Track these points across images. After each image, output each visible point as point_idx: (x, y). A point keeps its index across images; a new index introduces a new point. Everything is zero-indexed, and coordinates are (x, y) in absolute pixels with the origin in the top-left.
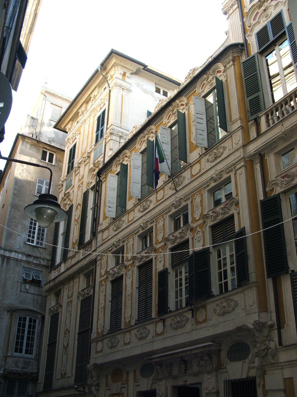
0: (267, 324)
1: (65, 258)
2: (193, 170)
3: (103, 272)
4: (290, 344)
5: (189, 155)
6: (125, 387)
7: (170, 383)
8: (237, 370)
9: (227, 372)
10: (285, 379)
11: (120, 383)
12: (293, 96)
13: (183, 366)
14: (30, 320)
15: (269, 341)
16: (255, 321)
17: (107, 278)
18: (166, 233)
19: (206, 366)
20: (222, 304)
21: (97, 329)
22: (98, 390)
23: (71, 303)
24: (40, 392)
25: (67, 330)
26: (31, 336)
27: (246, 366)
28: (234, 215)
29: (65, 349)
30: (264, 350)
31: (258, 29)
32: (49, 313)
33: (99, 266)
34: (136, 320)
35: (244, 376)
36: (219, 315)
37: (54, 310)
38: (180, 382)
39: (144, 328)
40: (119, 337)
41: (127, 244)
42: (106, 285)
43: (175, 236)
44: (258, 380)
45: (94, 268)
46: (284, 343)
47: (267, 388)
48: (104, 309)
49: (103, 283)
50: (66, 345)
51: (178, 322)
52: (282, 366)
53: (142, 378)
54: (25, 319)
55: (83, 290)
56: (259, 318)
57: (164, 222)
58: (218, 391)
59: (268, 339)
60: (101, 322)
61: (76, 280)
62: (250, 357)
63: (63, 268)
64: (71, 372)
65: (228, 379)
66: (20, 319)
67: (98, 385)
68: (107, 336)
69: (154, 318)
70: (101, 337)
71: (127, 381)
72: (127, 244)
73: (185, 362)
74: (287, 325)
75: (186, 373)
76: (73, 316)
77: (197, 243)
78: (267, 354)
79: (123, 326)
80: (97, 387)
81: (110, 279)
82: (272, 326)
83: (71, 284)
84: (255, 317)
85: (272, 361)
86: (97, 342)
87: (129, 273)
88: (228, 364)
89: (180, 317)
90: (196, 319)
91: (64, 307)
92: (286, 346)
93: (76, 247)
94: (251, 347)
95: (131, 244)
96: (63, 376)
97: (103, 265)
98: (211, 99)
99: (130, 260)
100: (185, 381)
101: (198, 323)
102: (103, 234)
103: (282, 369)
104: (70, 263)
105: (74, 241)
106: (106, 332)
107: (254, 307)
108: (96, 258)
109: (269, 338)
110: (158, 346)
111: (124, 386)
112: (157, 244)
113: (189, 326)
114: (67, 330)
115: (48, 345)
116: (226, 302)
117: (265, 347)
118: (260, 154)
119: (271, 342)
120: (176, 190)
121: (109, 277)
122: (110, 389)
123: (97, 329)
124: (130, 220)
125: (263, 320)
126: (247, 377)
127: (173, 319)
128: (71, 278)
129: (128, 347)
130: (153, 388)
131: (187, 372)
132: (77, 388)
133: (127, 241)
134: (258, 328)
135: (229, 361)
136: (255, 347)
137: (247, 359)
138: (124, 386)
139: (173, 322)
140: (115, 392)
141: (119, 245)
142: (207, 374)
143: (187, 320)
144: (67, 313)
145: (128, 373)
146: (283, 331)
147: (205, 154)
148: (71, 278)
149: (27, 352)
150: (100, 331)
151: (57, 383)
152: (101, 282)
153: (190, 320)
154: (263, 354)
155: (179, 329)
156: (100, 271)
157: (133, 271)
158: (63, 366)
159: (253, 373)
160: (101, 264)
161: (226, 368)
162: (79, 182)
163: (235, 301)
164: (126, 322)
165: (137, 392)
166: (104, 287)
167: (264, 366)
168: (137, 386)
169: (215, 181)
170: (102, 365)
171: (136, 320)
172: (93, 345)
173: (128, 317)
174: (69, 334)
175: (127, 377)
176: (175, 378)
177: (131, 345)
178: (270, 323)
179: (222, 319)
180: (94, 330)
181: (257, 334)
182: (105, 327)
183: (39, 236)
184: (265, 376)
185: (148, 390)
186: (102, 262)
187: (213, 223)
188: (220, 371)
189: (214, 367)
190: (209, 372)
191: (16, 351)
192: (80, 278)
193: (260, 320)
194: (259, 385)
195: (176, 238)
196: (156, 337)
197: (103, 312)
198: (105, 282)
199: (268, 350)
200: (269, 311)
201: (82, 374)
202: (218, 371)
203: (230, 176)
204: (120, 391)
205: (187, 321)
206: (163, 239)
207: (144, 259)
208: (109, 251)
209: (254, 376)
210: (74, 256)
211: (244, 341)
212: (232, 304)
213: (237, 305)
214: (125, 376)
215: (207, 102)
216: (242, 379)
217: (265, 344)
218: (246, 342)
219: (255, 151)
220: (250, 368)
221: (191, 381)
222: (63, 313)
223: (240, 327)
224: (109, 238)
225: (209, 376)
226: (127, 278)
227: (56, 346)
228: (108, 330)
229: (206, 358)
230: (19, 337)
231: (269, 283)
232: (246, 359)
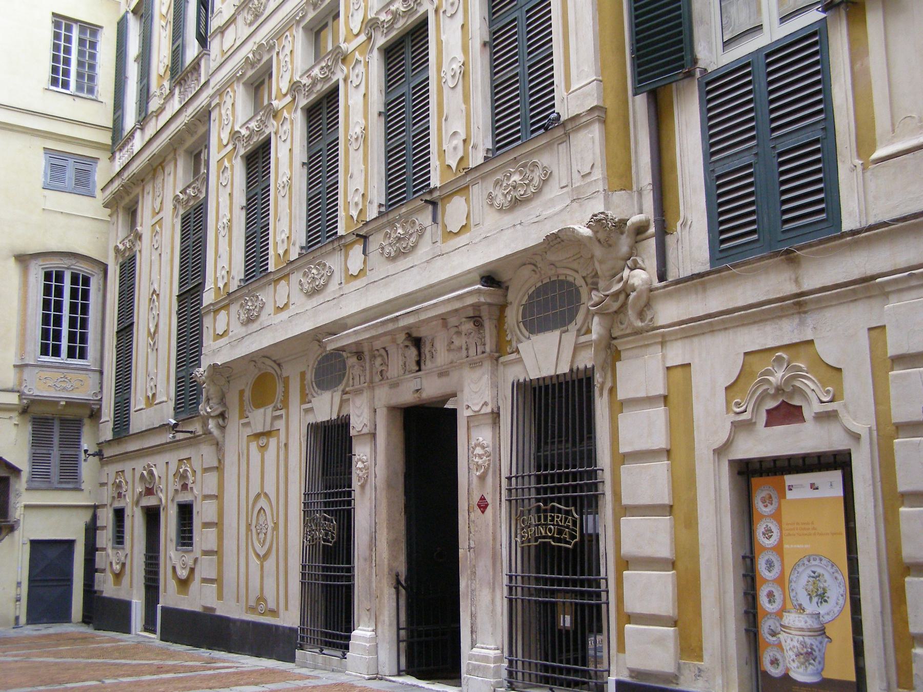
0: (629, 223)
1: (144, 118)
3: (225, 137)
4: (688, 273)
6: (281, 416)
7: (384, 396)
8: (545, 356)
9: (520, 360)
10: (668, 368)
11: (269, 409)
13: (413, 352)
14: (75, 279)
15: (632, 269)
16: (596, 215)
17: (235, 148)
18: (372, 8)
19: (467, 349)
20: (509, 178)
21: (216, 279)
22: (222, 428)
23: (161, 227)
24: (106, 442)
25: (154, 291)
26: (78, 330)
27: (570, 338)
29: (153, 339)
30: (616, 295)
32: (116, 257)
33: (217, 121)
34: (302, 248)
35: (564, 369)
36: (501, 210)
37: (125, 250)
38: (406, 396)
40: (262, 296)
41: (278, 54)
42: (232, 167)
43: (392, 13)
44: (598, 378)
46: (673, 274)
47: (621, 395)
48: (230, 229)
49: (226, 164)
50: (152, 330)
51: (399, 239)
52: (663, 335)
53: (319, 392)
54: (60, 277)
55: (183, 192)
56: (607, 206)
57: (293, 47)
58: (496, 410)
59: (629, 263)
60: (223, 262)
61: (170, 168)
62: (580, 317)
63: (137, 143)
64: (167, 392)
65: (521, 380)
66: (48, 276)
67: (222, 415)
69: (342, 237)
70: (228, 299)
71: (285, 404)
72: (278, 54)
73: (417, 342)
74: (684, 225)
75: (420, 370)
76: (166, 257)
77: (448, 21)
78: (624, 305)
79: (271, 268)
80: (221, 421)
82: (640, 230)
83: (159, 181)
84: (597, 206)
85: (639, 324)
86: (216, 311)
87: (285, 128)
88: (522, 338)
89: (403, 227)
91: (144, 237)
92: (678, 282)
93: (167, 84)
94: (584, 291)
95: (289, 53)
96: (151, 401)
97: (224, 117)
99: (357, 35)
100: (417, 391)
102: (223, 37)
103: (663, 344)
104: (152, 128)
105: (162, 72)
106: (476, 158)
107: (593, 178)
108: (209, 105)
109: (631, 260)
110: (351, 306)
111: (278, 413)
113: (425, 250)
114: (154, 291)
115: (117, 332)
116: (521, 173)
117: (621, 284)
119: (637, 271)
121: (239, 145)
122: (248, 424)
123: (216, 279)
124: (225, 48)
125: (615, 214)
126: (571, 370)
127: (387, 234)
128: (155, 168)
129: (284, 315)
130: (344, 413)
131: (423, 367)
132: (176, 425)
133: (279, 46)
134: (601, 236)
135: (527, 334)
136: (595, 287)
137: (574, 323)
138: (278, 413)
139: (387, 242)
140: (260, 429)
141: (259, 61)
143: (421, 233)
144: (154, 250)
145: (286, 381)
146: (670, 240)
148: (155, 168)
149: (71, 354)
151: (139, 421)
152: (220, 161)
153: (429, 229)
154: (615, 306)
155: (402, 258)
156: (219, 135)
157: (292, 123)
158: (149, 379)
159: (586, 360)
160: (220, 115)
161: (517, 351)
163: (544, 168)
166: (229, 172)
167: (615, 338)
169: (253, 65)
170: (227, 366)
171: (302, 248)
172: (207, 322)
173: (283, 241)
174: (158, 301)
176: (395, 385)
177: (292, 310)
178: (635, 219)
179: (508, 219)
180: (209, 284)
181: (598, 252)
182: (233, 273)
183: (81, 70)
184: (618, 364)
186: (223, 112)
188: (502, 359)
189: (488, 349)
190: (474, 365)
191: (44, 351)
192: (176, 160)
193: (610, 213)
194: (601, 390)
195: (396, 16)
197: (227, 238)
198: (230, 161)
199: (628, 295)
200: (635, 188)
201: (188, 395)
202: (497, 359)
204: (272, 424)
205: (421, 236)
207: (319, 87)
208: (239, 79)
209: (589, 366)
210: (162, 109)
211: (566, 276)
212: (537, 175)
213: (547, 177)
214: (280, 388)
216: (558, 376)
217: (622, 279)
218: (570, 279)
220: (577, 348)
221: (430, 388)
222: (144, 252)
223: (555, 236)
225: (478, 373)
226: (280, 143)
227: (132, 334)
228: (240, 280)
229: (468, 326)
230: (51, 321)
231: (640, 105)
232: (570, 322)
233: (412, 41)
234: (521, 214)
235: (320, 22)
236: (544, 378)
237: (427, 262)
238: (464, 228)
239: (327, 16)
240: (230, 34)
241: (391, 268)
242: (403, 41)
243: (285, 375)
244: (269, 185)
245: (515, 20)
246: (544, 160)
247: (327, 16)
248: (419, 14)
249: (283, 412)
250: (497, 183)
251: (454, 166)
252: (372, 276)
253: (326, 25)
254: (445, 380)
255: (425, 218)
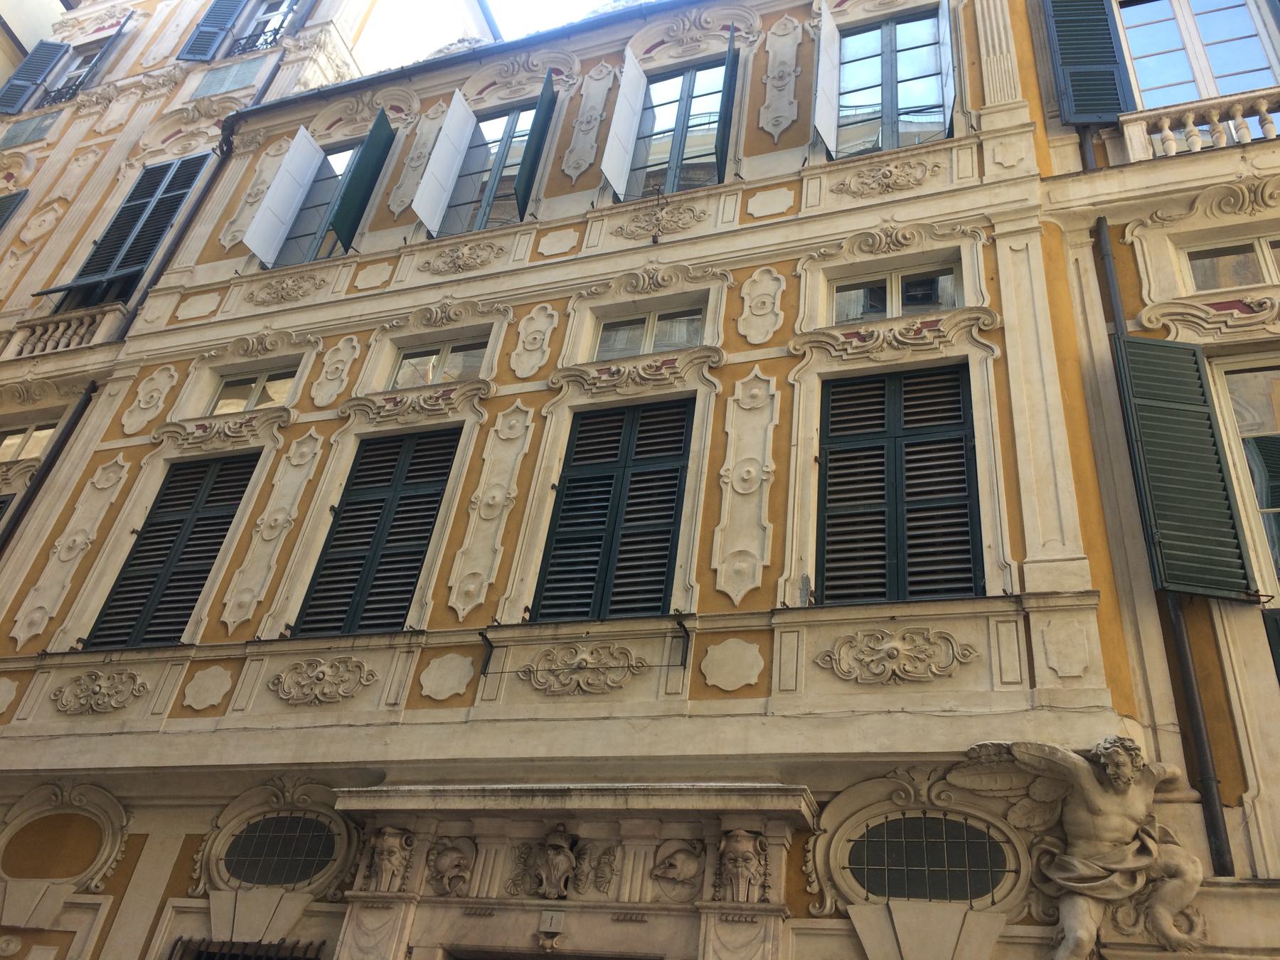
2: (362, 274)
5: (366, 231)
9: (206, 912)
12: (1239, 109)
19: (764, 887)
28: (967, 364)
31: (153, 162)
35: (273, 938)
39: (344, 661)
45: (65, 408)
53: (235, 882)
68: (68, 660)
71: (118, 884)
72: (320, 355)
79: (193, 633)
81: (174, 454)
90: (700, 674)
98: (341, 163)
101: (703, 688)
106: (268, 630)
112: (303, 411)
118: (1101, 221)
120: (655, 241)
142: (721, 920)
145: (136, 845)
147: (252, 279)
150: (230, 617)
160: (133, 393)
162: (86, 138)
164: (225, 624)
165: (180, 939)
167: (1105, 946)
168: (180, 911)
169: (429, 322)
171: (288, 627)
175: (125, 868)
176: (481, 910)
179: (61, 725)
185: (265, 942)
186: (142, 389)
187: (377, 429)
196: (408, 706)
203: (300, 357)
206: (342, 400)
214: (110, 853)
215: (325, 165)
219: (1093, 204)
224: (213, 320)
228: (79, 640)
233: (222, 470)
234: (902, 696)
235: (286, 367)
236: (246, 944)
237: (653, 718)
238: (213, 710)
239: (261, 371)
240: (199, 307)
241: (545, 708)
242: (623, 414)
243: (135, 827)
244: (233, 516)
245: (382, 501)
246: (370, 663)
247: (261, 371)
248: (443, 421)
249: (107, 902)
250: (295, 668)
251: (461, 614)
252: (481, 709)
253: (254, 380)
254: (632, 929)
255: (655, 654)
